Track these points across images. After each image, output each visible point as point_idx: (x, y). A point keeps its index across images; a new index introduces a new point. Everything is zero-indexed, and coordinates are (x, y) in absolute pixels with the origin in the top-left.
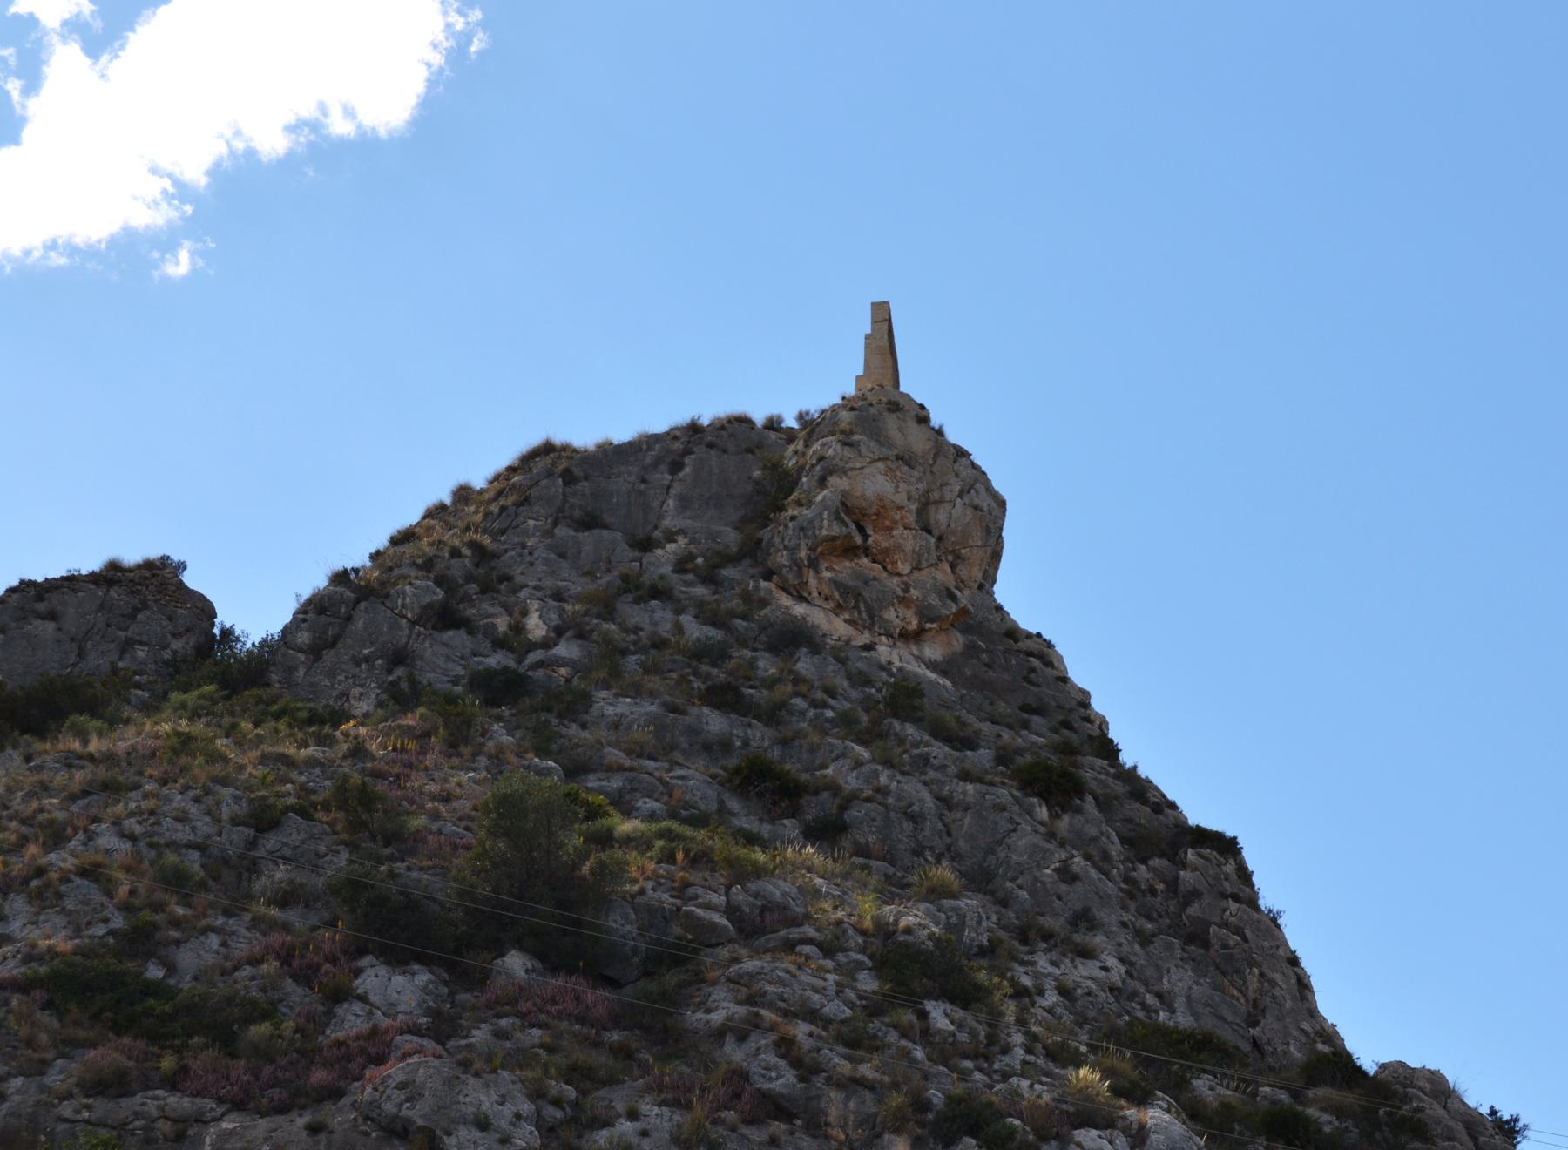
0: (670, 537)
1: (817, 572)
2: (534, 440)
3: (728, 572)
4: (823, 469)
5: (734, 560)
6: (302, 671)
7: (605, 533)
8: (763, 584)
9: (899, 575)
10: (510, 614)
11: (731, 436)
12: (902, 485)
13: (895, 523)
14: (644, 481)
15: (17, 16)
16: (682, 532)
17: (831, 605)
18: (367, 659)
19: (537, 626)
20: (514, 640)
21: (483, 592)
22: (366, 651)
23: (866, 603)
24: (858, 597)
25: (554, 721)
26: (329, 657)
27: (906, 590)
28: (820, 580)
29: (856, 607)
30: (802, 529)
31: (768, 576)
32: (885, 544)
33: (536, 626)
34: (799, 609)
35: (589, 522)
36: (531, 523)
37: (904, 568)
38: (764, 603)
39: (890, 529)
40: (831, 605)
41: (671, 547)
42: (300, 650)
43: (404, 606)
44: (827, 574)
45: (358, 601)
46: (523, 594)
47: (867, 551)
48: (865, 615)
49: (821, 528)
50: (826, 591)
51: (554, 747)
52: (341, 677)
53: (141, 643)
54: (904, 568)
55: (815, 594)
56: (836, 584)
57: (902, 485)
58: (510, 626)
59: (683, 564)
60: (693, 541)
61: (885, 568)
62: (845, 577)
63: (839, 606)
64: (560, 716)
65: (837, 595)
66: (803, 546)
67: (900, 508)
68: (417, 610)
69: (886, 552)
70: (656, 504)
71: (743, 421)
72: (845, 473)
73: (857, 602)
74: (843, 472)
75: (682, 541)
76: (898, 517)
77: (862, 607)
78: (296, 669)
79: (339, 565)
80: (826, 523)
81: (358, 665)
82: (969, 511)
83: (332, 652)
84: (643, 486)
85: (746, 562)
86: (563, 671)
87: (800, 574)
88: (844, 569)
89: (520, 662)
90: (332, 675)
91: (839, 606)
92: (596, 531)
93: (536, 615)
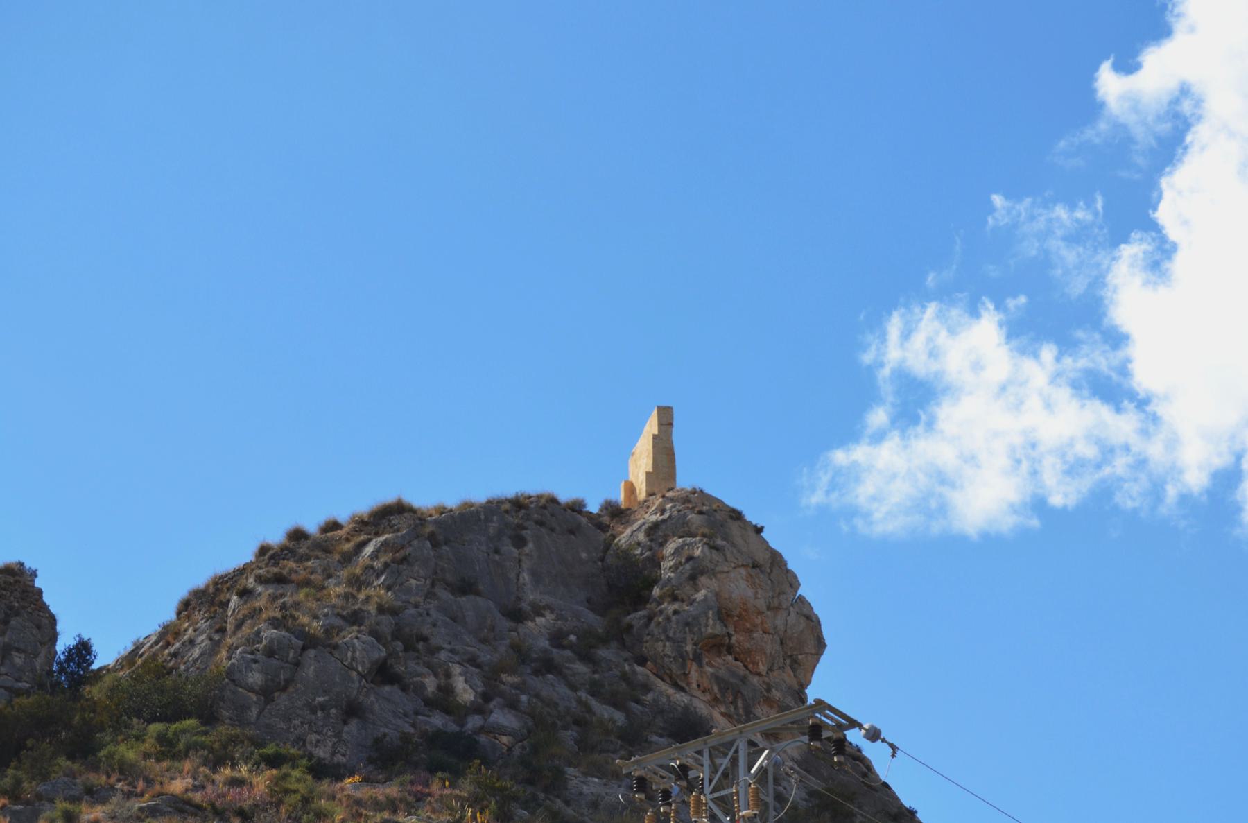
0: (538, 611)
1: (700, 665)
2: (387, 496)
3: (602, 653)
4: (693, 568)
5: (604, 641)
6: (254, 712)
7: (479, 599)
8: (639, 669)
9: (759, 674)
10: (436, 675)
11: (552, 515)
12: (760, 591)
13: (755, 626)
14: (497, 551)
15: (1108, 59)
16: (550, 608)
17: (708, 697)
18: (323, 707)
19: (465, 690)
20: (444, 701)
21: (406, 650)
22: (321, 699)
23: (744, 700)
24: (737, 693)
25: (542, 796)
26: (282, 700)
27: (769, 690)
28: (702, 673)
29: (734, 703)
30: (687, 624)
31: (642, 661)
32: (747, 645)
33: (465, 692)
34: (680, 698)
35: (465, 588)
36: (413, 582)
37: (762, 668)
38: (647, 688)
39: (750, 631)
40: (708, 697)
41: (539, 620)
42: (251, 690)
43: (353, 659)
44: (709, 670)
45: (304, 649)
46: (443, 655)
47: (730, 650)
48: (741, 711)
49: (707, 626)
50: (706, 683)
51: (181, 746)
52: (297, 722)
53: (18, 650)
54: (762, 668)
55: (694, 686)
56: (717, 679)
57: (760, 591)
58: (439, 688)
59: (557, 639)
60: (560, 617)
61: (746, 667)
62: (722, 672)
63: (716, 699)
64: (546, 790)
65: (716, 689)
66: (689, 640)
67: (760, 613)
68: (368, 665)
69: (748, 652)
70: (512, 576)
71: (553, 500)
72: (714, 574)
73: (735, 698)
74: (713, 573)
75: (550, 617)
76: (758, 621)
77: (740, 703)
78: (249, 708)
79: (22, 560)
80: (711, 622)
81: (314, 712)
82: (802, 620)
83: (284, 696)
84: (497, 557)
85: (614, 644)
86: (505, 739)
87: (683, 666)
88: (723, 664)
89: (462, 726)
90: (288, 719)
91: (716, 699)
92: (472, 597)
93: (461, 679)
